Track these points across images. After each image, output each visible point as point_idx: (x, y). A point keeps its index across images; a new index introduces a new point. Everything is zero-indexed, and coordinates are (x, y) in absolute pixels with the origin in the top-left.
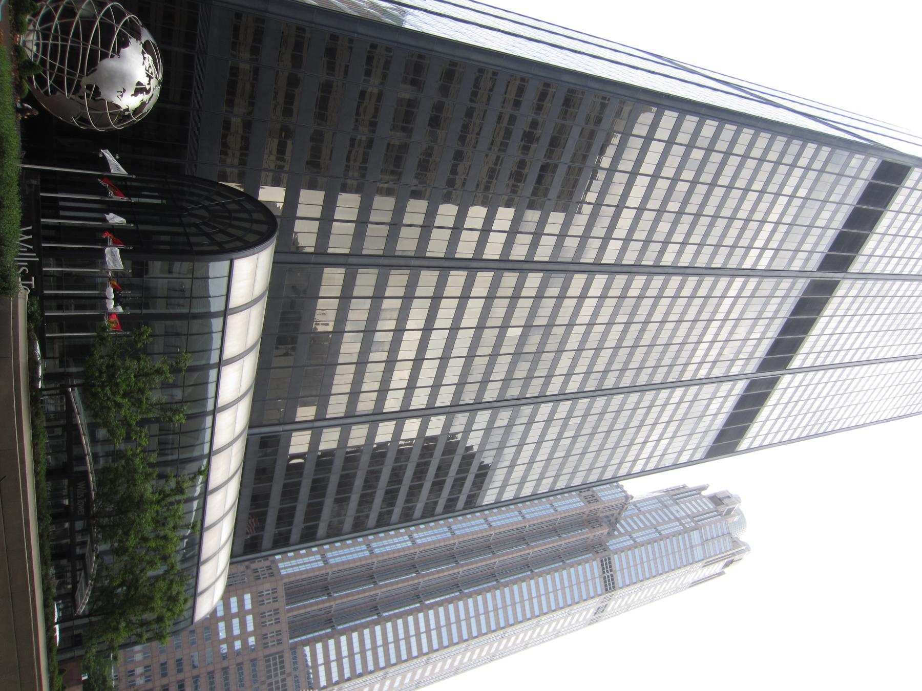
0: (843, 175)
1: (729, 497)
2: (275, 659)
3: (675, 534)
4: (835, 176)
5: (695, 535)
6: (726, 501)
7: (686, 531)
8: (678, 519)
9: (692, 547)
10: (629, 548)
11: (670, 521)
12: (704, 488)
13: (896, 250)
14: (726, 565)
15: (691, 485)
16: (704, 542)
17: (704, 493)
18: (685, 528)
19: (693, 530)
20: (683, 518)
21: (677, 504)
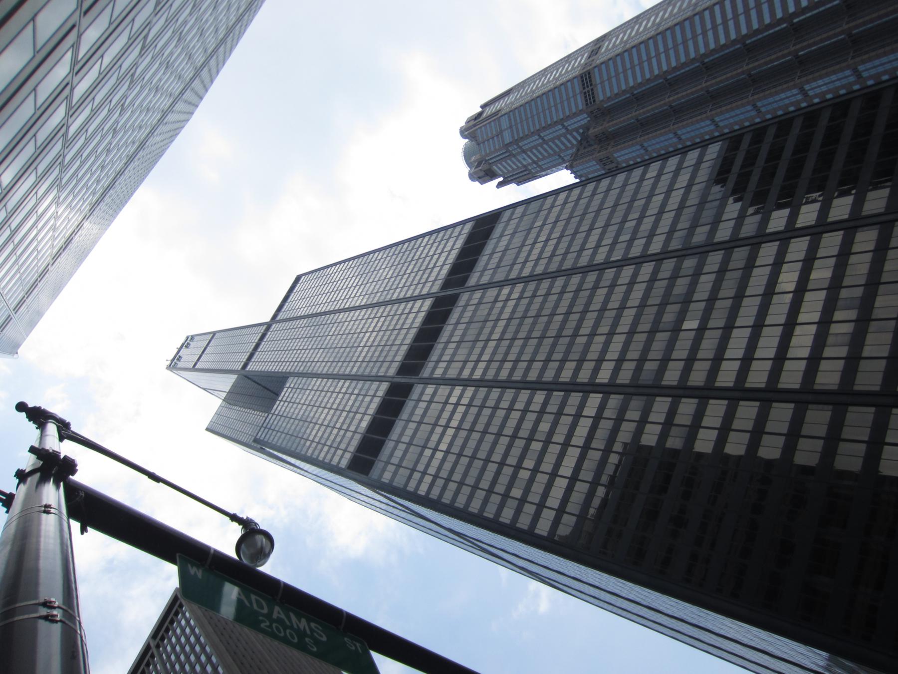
1: (480, 178)
7: (515, 142)
8: (524, 152)
11: (530, 150)
12: (500, 185)
16: (500, 133)
17: (501, 179)
18: (517, 145)
19: (511, 143)
20: (518, 153)
21: (525, 166)
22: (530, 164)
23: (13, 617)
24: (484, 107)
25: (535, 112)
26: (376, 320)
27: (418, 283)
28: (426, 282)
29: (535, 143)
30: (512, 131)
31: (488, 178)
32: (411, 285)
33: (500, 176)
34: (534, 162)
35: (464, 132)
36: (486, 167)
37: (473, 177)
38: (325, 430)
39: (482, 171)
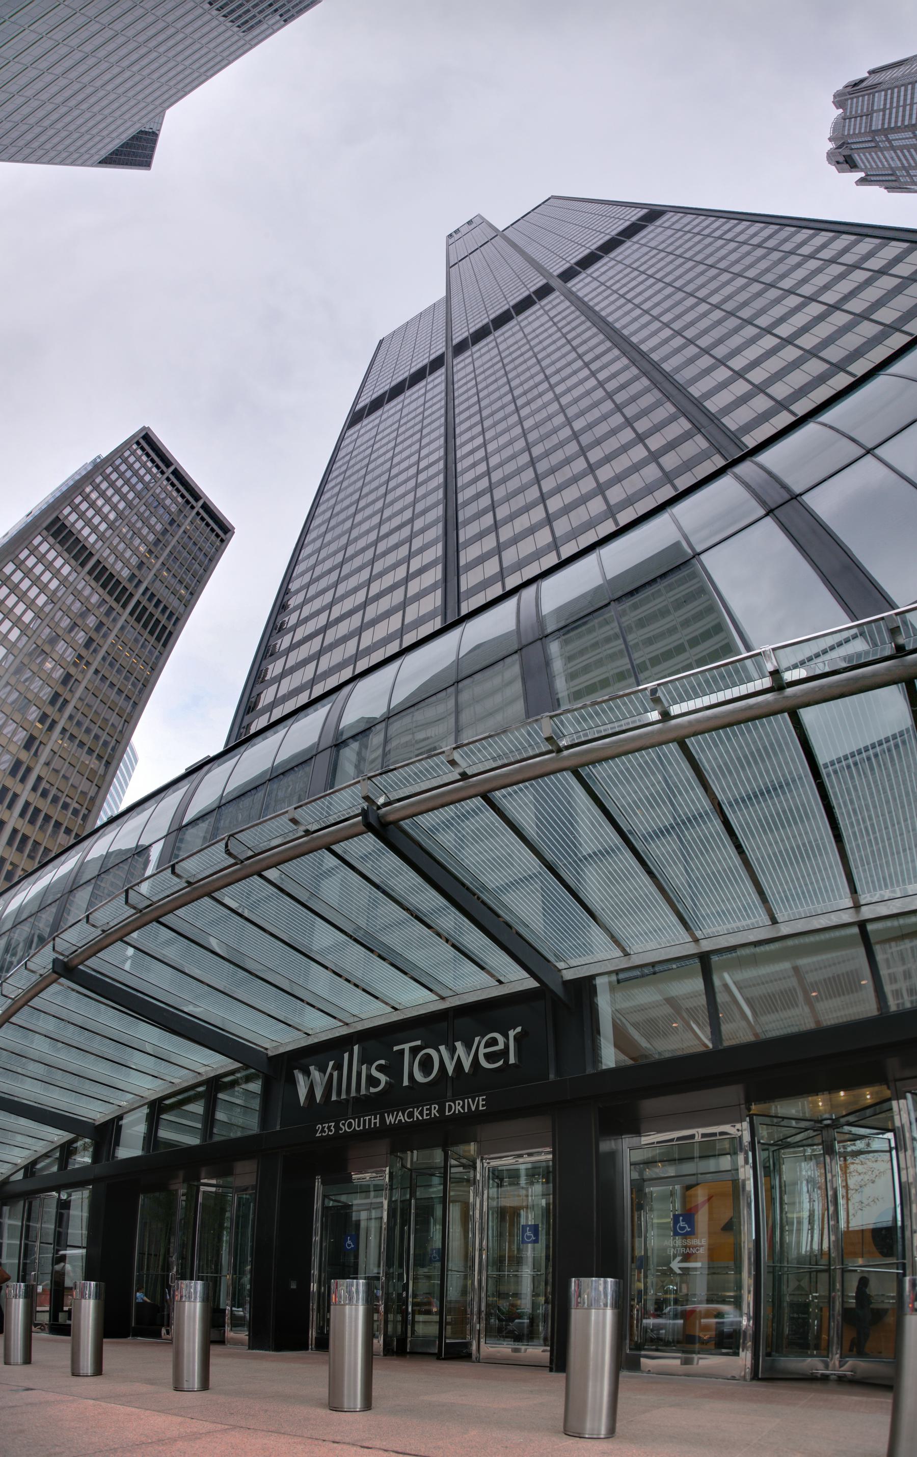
0: (707, 353)
1: (838, 163)
2: (125, 461)
3: (896, 129)
4: (729, 363)
5: (877, 124)
6: (841, 159)
7: (885, 132)
8: (893, 148)
9: (884, 110)
10: (896, 129)
11: (901, 148)
12: (862, 181)
13: (759, 294)
14: (862, 81)
15: (877, 192)
16: (869, 115)
17: (862, 174)
18: (886, 136)
19: (878, 131)
20: (886, 149)
21: (891, 168)
22: (898, 168)
23: (215, 1193)
24: (872, 72)
25: (901, 103)
26: (740, 282)
27: (833, 261)
28: (882, 272)
29: (907, 142)
30: (884, 115)
31: (846, 166)
32: (811, 256)
33: (862, 170)
34: (904, 167)
35: (840, 100)
36: (847, 152)
37: (831, 157)
38: (640, 316)
39: (844, 159)
